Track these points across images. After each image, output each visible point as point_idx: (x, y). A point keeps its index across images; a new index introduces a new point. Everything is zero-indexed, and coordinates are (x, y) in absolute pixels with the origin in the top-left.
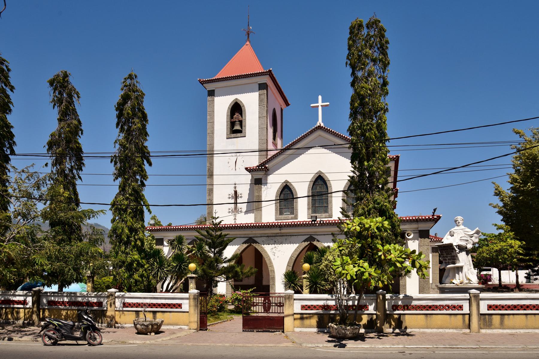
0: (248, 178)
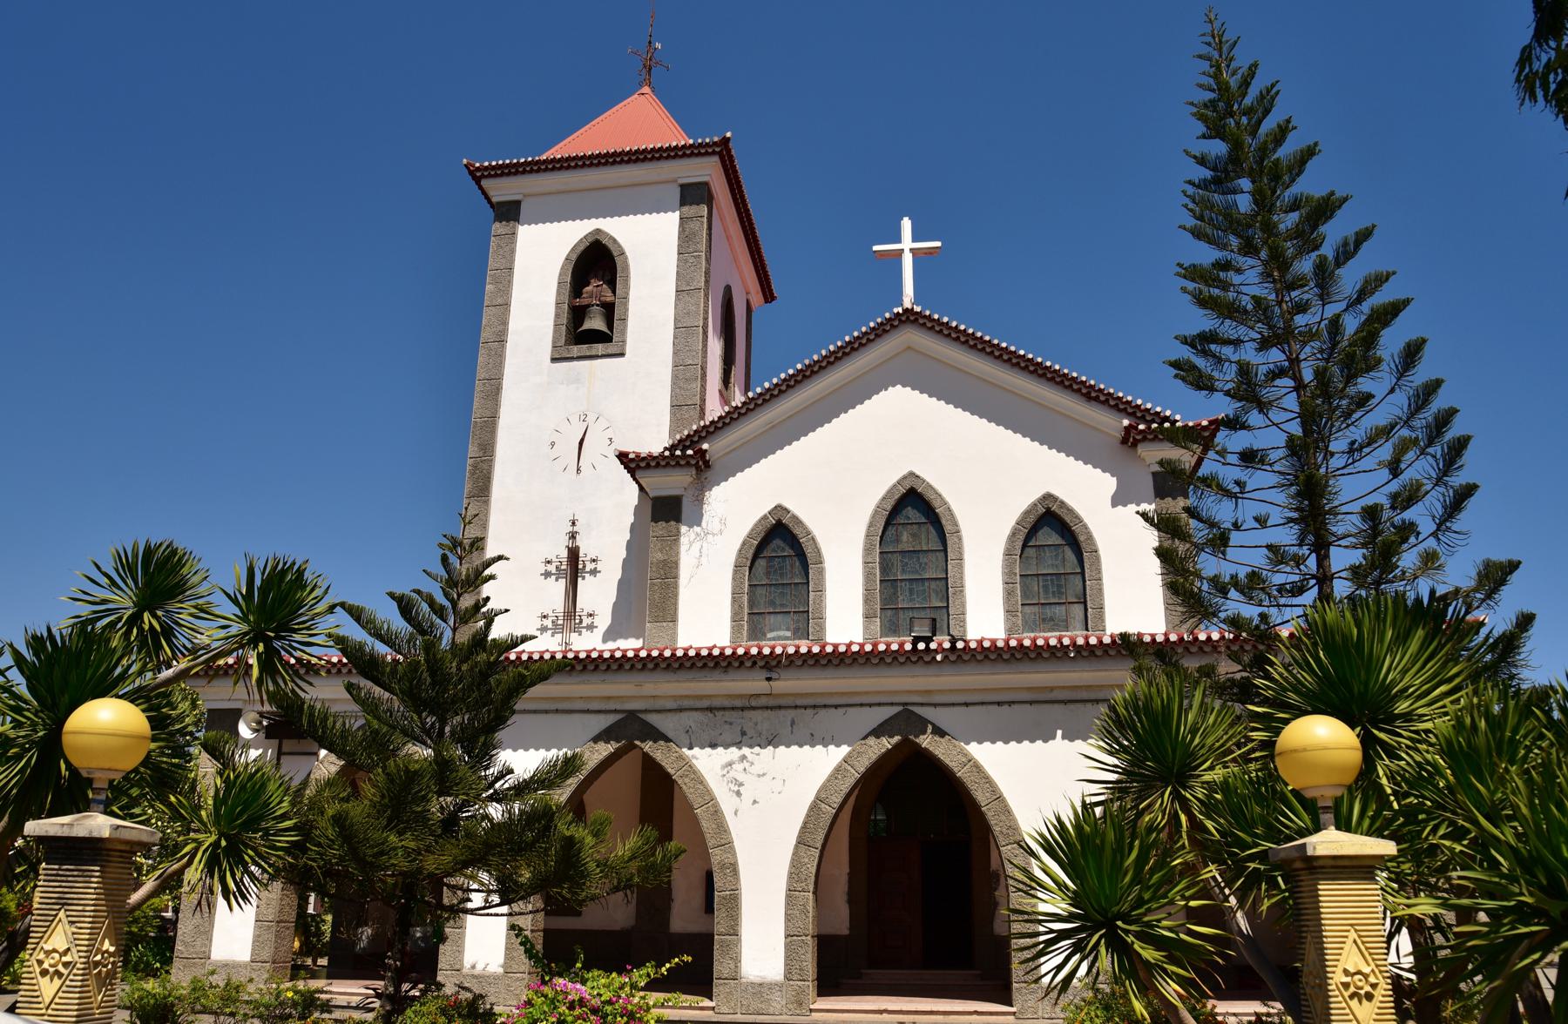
0: (621, 497)
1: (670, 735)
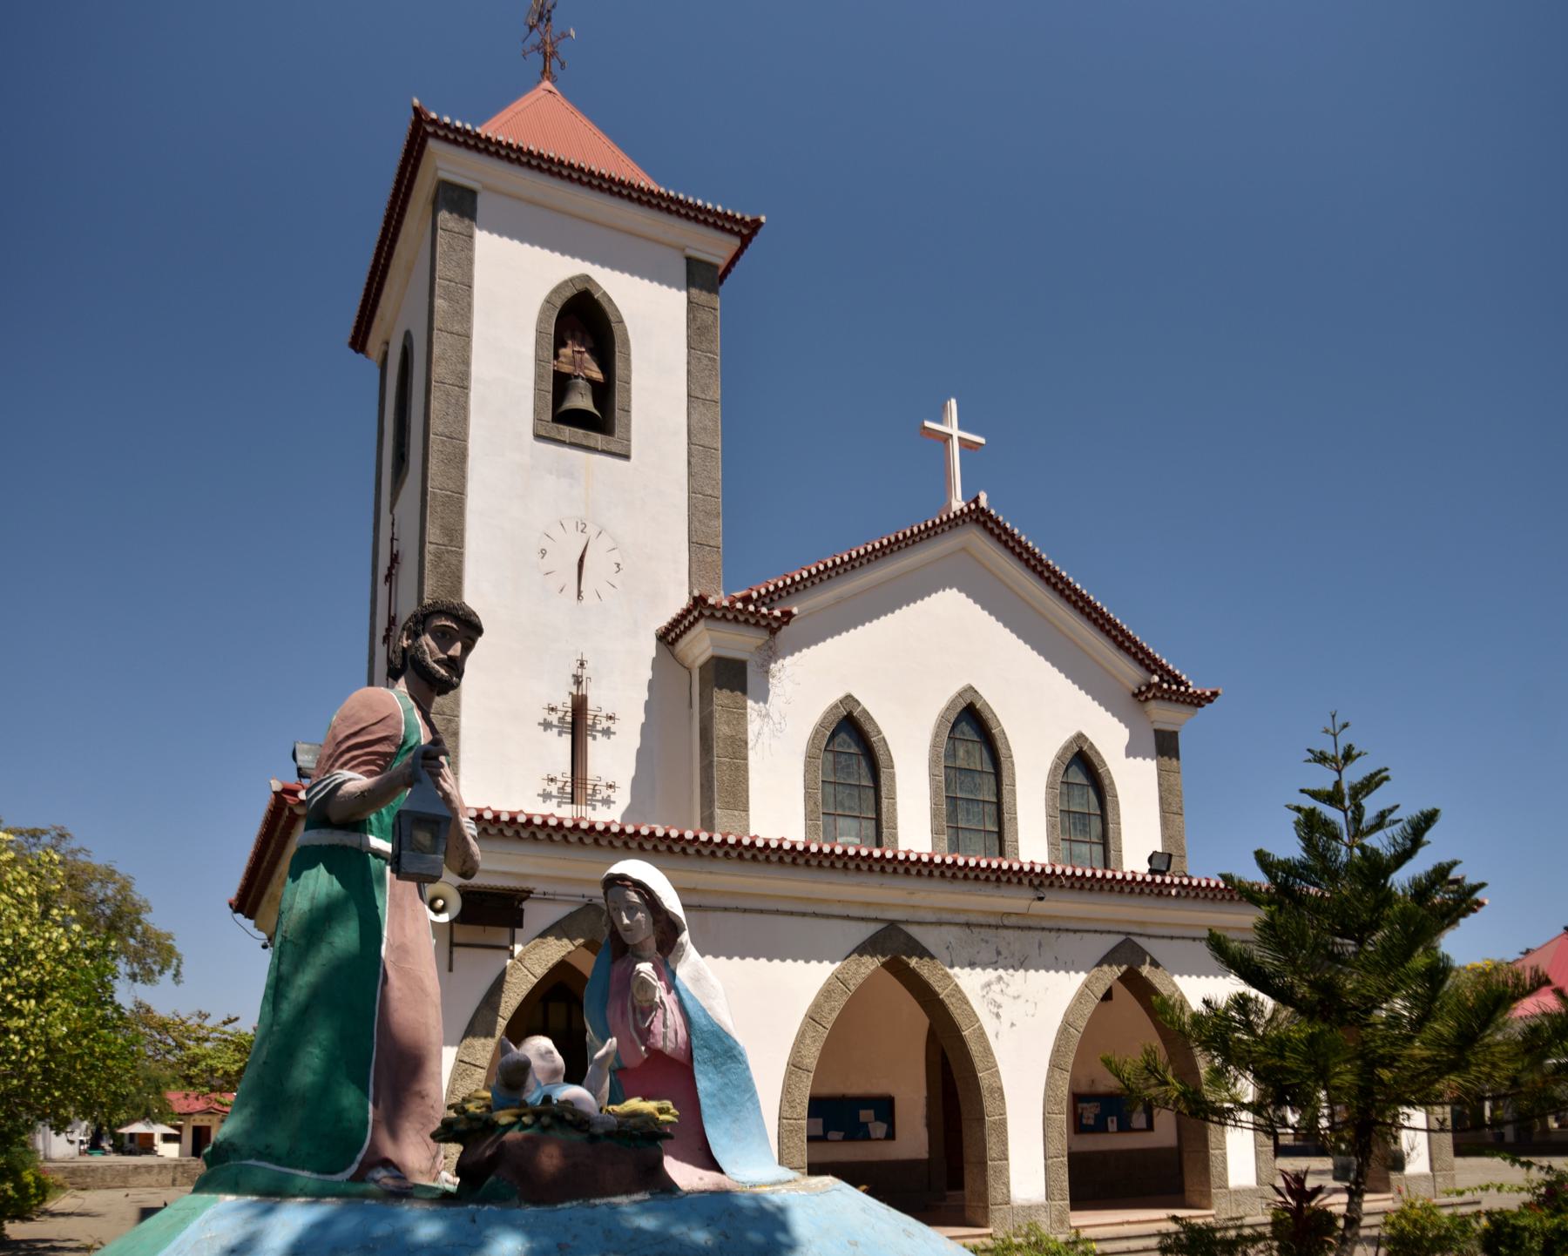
1: (932, 950)
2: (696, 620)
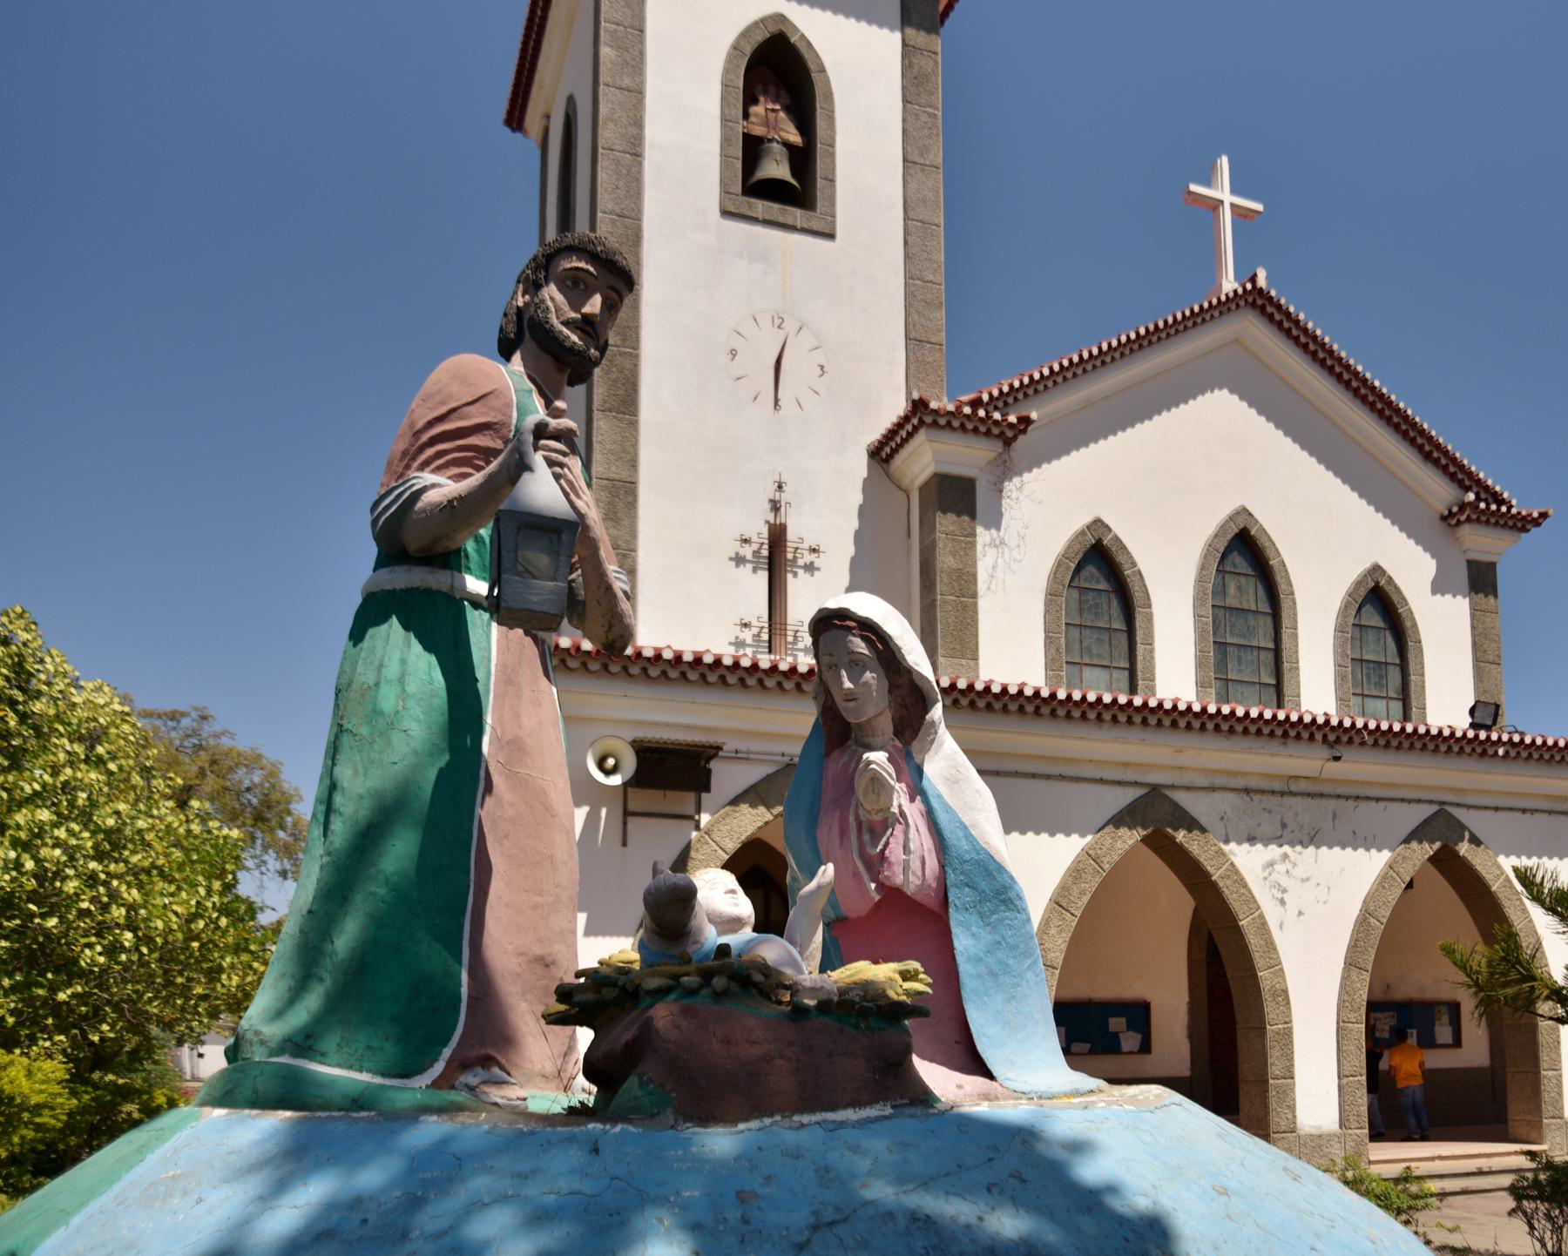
1: (1203, 821)
2: (916, 429)
